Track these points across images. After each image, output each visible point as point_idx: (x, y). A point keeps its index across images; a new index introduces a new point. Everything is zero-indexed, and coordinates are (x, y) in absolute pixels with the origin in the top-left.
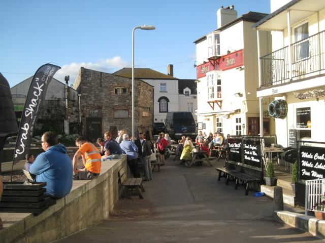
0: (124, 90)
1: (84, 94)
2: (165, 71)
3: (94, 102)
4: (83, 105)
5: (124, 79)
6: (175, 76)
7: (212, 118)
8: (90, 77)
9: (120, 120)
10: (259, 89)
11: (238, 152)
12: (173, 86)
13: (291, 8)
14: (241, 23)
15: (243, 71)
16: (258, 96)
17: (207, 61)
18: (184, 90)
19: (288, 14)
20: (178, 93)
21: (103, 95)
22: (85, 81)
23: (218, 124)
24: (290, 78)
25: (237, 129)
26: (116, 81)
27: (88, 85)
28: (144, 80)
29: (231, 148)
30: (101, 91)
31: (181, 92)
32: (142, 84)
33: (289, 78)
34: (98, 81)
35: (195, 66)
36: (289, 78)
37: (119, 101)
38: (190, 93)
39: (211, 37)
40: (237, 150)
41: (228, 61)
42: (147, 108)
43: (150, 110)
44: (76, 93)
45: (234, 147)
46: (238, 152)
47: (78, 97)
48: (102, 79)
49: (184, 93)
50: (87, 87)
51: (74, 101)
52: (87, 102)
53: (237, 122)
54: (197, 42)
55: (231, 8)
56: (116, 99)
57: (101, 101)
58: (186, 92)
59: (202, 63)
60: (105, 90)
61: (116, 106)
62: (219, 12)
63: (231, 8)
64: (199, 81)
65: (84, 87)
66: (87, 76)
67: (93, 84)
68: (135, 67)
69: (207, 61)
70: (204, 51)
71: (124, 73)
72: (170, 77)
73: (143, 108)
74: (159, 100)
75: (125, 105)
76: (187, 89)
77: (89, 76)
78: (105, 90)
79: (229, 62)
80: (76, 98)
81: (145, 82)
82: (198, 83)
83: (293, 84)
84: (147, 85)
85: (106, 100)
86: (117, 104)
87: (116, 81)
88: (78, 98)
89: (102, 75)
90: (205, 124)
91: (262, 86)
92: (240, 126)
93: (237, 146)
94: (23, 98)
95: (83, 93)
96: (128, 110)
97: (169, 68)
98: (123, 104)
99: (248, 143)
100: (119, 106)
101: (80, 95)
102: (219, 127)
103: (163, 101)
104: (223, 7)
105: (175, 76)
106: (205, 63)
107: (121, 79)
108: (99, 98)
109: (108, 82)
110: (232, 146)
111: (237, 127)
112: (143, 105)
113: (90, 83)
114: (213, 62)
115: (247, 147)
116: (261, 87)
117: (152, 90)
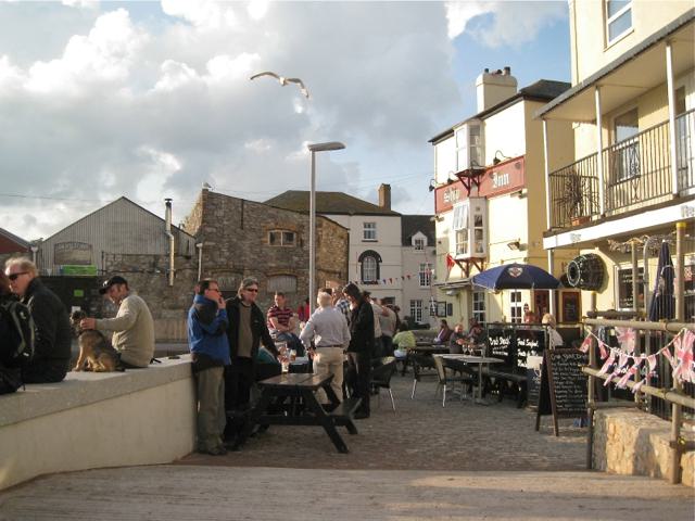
0: (289, 237)
1: (207, 243)
2: (375, 199)
3: (228, 259)
4: (206, 264)
5: (289, 213)
6: (393, 208)
7: (464, 295)
8: (221, 208)
9: (546, 465)
10: (546, 235)
11: (506, 354)
12: (389, 230)
13: (602, 82)
14: (520, 106)
15: (525, 200)
16: (545, 247)
17: (455, 178)
18: (414, 238)
19: (597, 93)
20: (400, 244)
21: (246, 245)
22: (209, 218)
23: (476, 304)
24: (675, 192)
25: (513, 315)
26: (272, 216)
27: (217, 225)
28: (329, 217)
29: (493, 346)
30: (243, 238)
31: (406, 241)
32: (324, 225)
33: (670, 193)
34: (237, 218)
35: (431, 188)
36: (670, 193)
37: (277, 259)
38: (425, 243)
39: (462, 134)
40: (505, 350)
41: (495, 179)
42: (335, 273)
43: (340, 277)
44: (192, 241)
45: (498, 346)
46: (506, 354)
47: (197, 249)
48: (245, 214)
49: (413, 243)
50: (214, 230)
51: (188, 258)
52: (212, 260)
53: (513, 300)
54: (435, 141)
55: (504, 72)
56: (272, 254)
57: (243, 258)
58: (416, 241)
59: (446, 182)
60: (250, 235)
61: (271, 268)
62: (480, 79)
63: (504, 72)
64: (440, 220)
65: (209, 230)
66: (214, 207)
67: (225, 223)
68: (317, 190)
69: (455, 178)
70: (451, 158)
71: (293, 201)
72: (385, 211)
73: (328, 272)
74: (361, 259)
75: (290, 268)
76: (419, 236)
77: (217, 206)
78: (250, 235)
79: (500, 179)
80: (192, 252)
81: (330, 220)
82: (437, 224)
83: (607, 224)
84: (334, 225)
85: (252, 256)
86: (273, 265)
87: (272, 216)
88: (197, 252)
89: (245, 206)
90: (451, 305)
91: (551, 228)
92: (519, 309)
93: (505, 342)
94: (85, 250)
95: (206, 240)
96: (296, 277)
97: (382, 193)
98: (286, 264)
99: (525, 335)
100: (278, 268)
101: (200, 245)
102: (479, 311)
103: (369, 262)
104: (487, 70)
105: (393, 208)
106: (450, 182)
107: (282, 214)
108: (238, 252)
109: (256, 219)
110: (495, 342)
111: (513, 309)
112: (327, 267)
113: (219, 220)
114: (466, 181)
115: (522, 343)
116: (550, 230)
117: (345, 236)
